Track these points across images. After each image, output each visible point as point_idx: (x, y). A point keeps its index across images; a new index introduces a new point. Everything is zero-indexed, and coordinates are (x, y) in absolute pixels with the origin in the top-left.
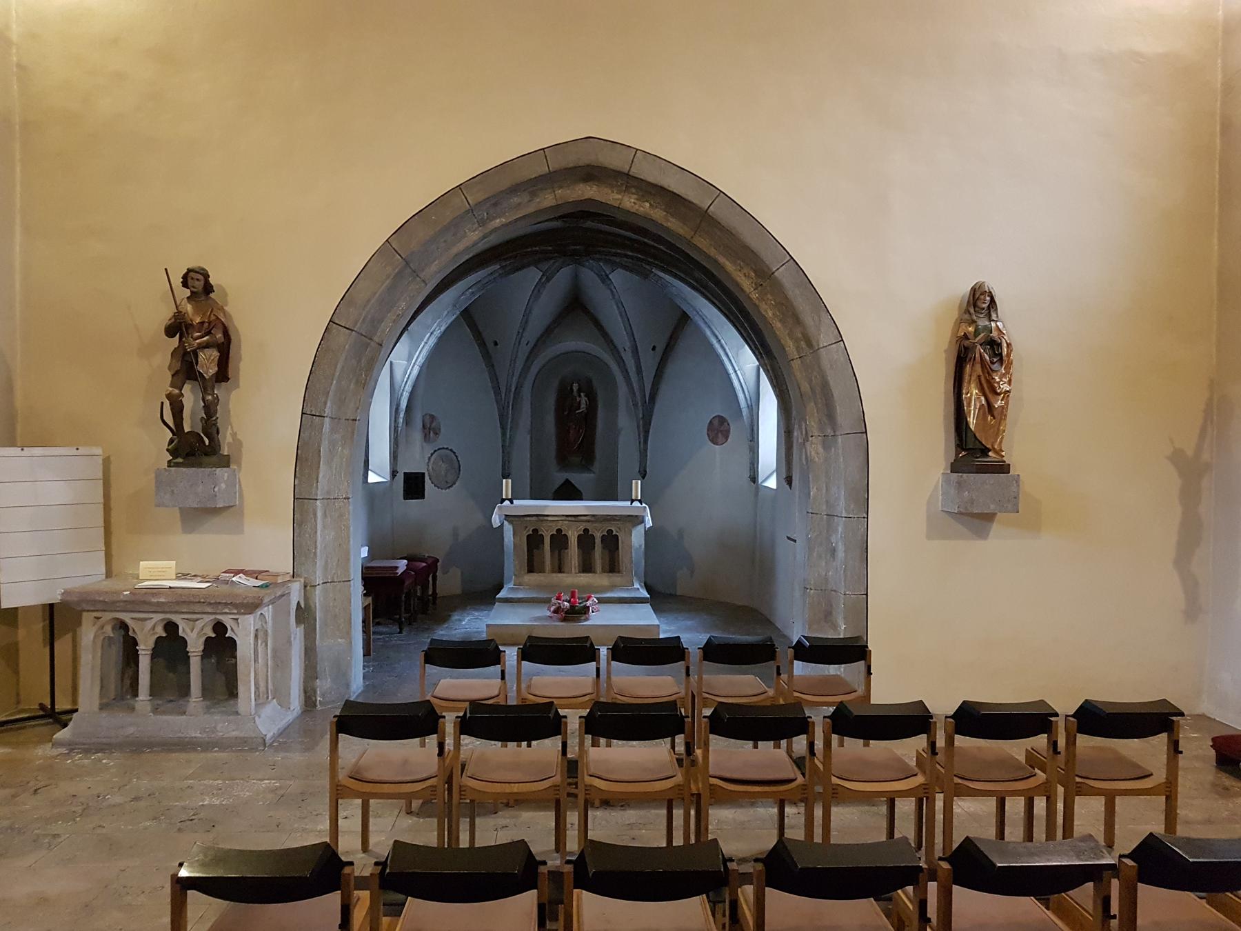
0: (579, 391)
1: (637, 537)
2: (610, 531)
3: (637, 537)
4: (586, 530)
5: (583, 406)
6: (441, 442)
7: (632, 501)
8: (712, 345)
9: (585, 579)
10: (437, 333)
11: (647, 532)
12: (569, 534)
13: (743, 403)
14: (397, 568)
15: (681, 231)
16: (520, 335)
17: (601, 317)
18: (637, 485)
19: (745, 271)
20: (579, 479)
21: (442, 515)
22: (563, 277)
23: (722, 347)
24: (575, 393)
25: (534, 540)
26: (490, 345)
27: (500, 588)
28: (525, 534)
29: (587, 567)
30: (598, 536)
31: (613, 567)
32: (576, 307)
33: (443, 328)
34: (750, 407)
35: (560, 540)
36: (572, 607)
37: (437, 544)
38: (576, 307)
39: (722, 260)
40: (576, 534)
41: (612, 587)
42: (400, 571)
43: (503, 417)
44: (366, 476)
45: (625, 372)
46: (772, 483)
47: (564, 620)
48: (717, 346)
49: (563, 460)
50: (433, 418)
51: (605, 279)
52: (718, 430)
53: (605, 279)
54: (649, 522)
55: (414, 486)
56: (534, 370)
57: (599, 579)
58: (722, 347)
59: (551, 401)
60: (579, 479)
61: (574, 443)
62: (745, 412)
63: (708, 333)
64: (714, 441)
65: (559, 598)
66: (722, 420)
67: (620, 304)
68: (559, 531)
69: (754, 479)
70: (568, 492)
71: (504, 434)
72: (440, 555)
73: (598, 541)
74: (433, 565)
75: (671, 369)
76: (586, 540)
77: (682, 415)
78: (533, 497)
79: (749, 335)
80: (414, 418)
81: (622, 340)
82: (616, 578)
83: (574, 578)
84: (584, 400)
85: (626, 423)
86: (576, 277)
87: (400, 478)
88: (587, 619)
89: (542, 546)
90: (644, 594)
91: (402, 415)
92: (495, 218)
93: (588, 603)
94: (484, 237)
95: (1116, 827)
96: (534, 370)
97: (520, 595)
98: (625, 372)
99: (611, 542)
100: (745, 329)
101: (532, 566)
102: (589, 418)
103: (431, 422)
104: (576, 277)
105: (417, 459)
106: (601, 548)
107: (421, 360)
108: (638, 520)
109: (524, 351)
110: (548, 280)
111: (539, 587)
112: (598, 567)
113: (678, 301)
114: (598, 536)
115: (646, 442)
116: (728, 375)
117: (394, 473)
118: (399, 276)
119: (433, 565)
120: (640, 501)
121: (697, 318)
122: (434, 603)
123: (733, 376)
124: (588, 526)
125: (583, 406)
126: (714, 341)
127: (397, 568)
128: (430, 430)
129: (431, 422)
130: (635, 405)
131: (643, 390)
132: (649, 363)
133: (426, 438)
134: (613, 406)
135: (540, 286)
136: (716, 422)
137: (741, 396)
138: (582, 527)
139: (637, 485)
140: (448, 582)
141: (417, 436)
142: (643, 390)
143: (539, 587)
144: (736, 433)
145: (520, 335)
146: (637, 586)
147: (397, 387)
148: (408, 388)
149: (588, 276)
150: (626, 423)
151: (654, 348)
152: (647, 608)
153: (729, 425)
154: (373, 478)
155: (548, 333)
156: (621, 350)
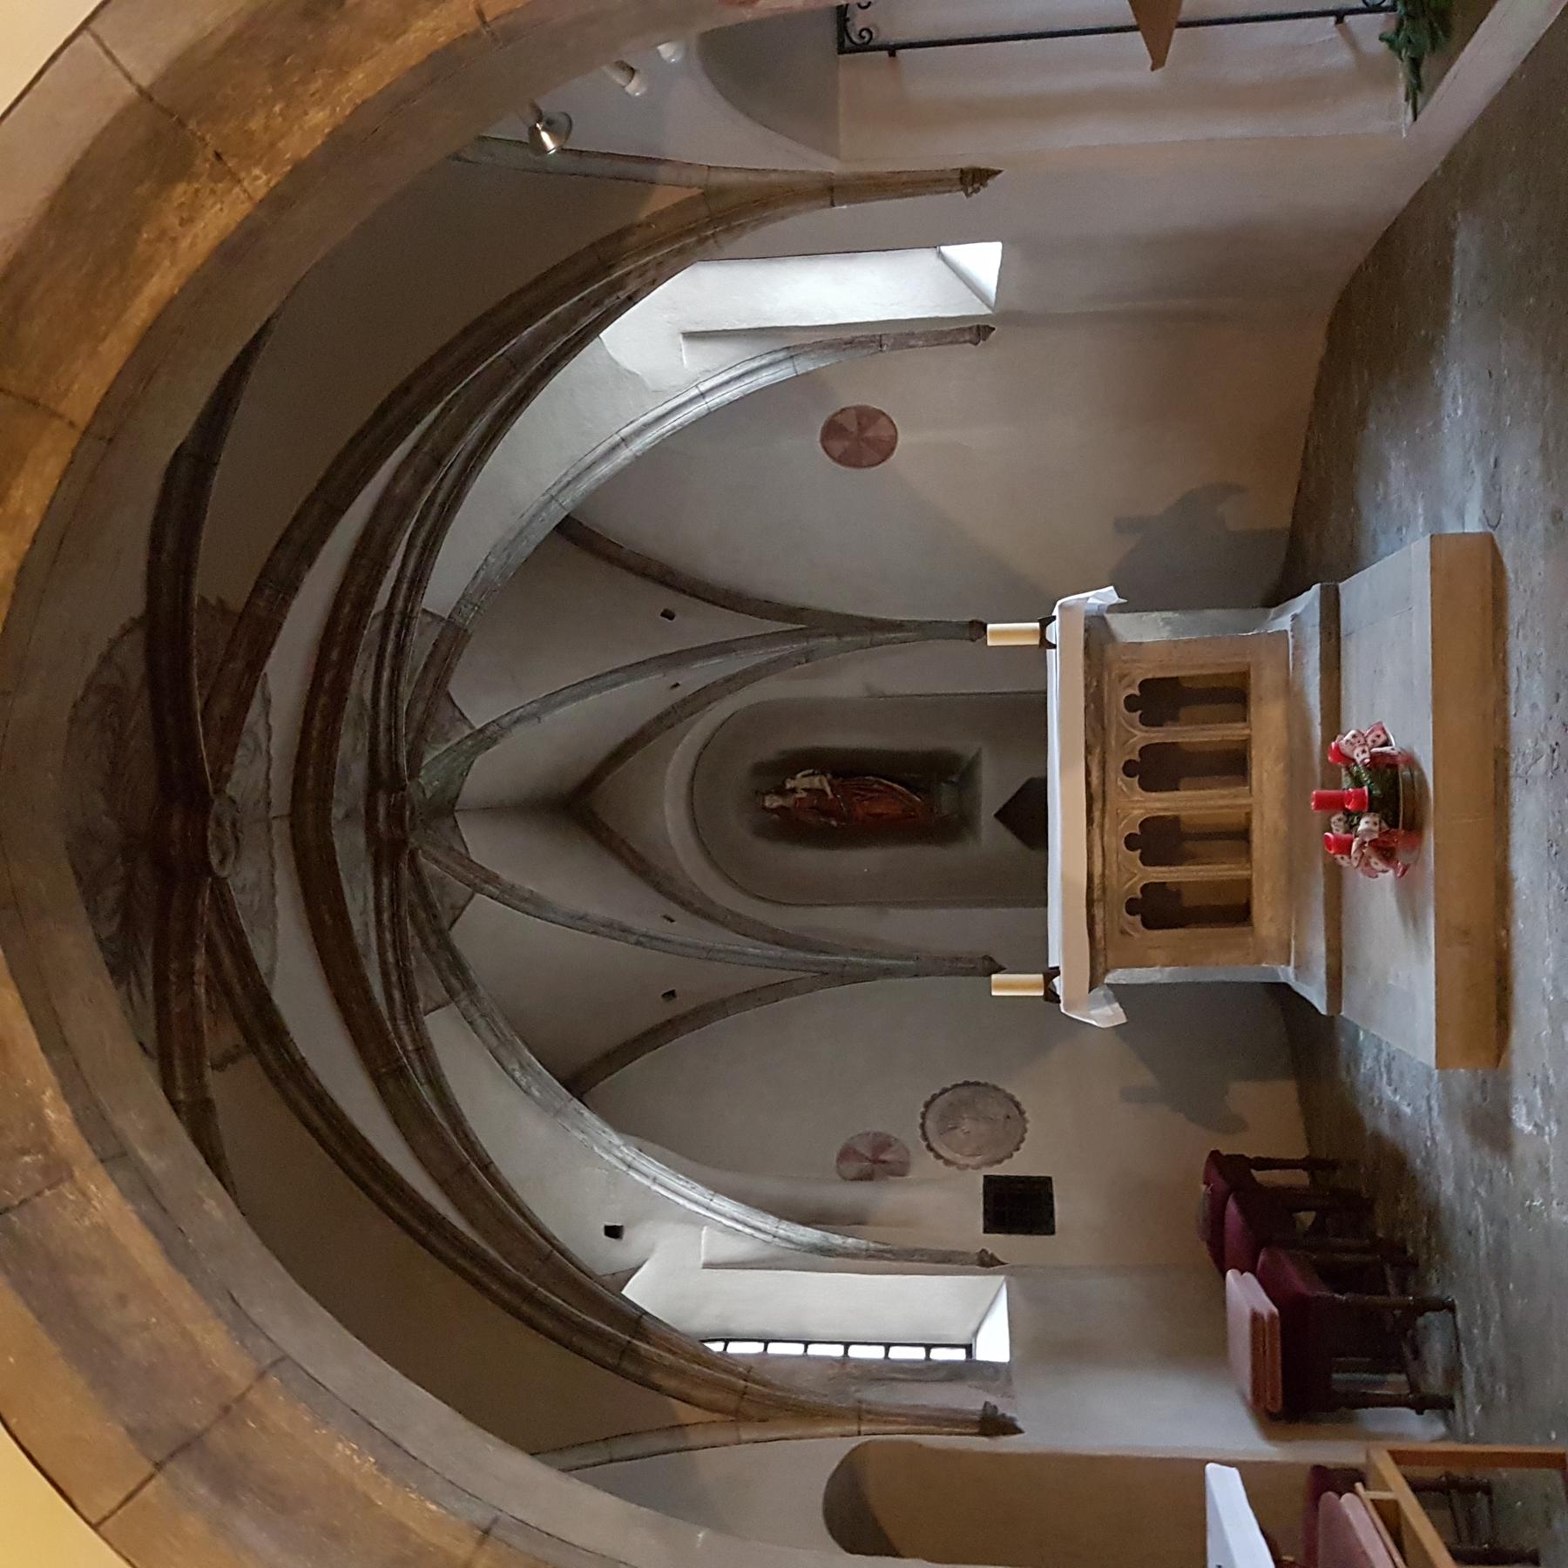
0: (781, 791)
1: (1146, 632)
2: (1131, 703)
3: (1146, 632)
4: (1129, 769)
5: (816, 782)
6: (910, 1136)
7: (1046, 644)
8: (638, 459)
9: (1267, 769)
10: (629, 1153)
11: (1134, 602)
12: (1139, 814)
13: (784, 372)
14: (1256, 1318)
15: (53, 468)
16: (645, 941)
17: (601, 753)
18: (1005, 633)
19: (172, 220)
20: (993, 789)
21: (1097, 1140)
22: (482, 843)
23: (639, 432)
24: (789, 802)
25: (1159, 909)
26: (681, 1006)
27: (1282, 994)
28: (1140, 934)
29: (1233, 764)
30: (1142, 736)
31: (1232, 694)
32: (579, 807)
33: (616, 1140)
34: (793, 353)
35: (1156, 841)
36: (1373, 805)
37: (1175, 1151)
38: (579, 807)
39: (140, 312)
40: (1139, 795)
41: (1291, 692)
42: (1266, 1306)
43: (845, 976)
44: (992, 1370)
45: (732, 683)
46: (982, 261)
47: (1414, 827)
48: (637, 446)
49: (951, 828)
50: (846, 1154)
51: (485, 739)
52: (858, 439)
53: (485, 739)
54: (1107, 596)
55: (1018, 1206)
56: (726, 897)
57: (1267, 729)
58: (639, 432)
59: (810, 860)
60: (993, 789)
61: (907, 799)
62: (805, 365)
63: (604, 469)
64: (885, 449)
65: (1344, 847)
66: (832, 430)
67: (551, 701)
68: (1130, 842)
69: (978, 331)
70: (1027, 815)
71: (888, 972)
72: (1199, 1144)
73: (1158, 735)
74: (1230, 1173)
75: (717, 568)
76: (1154, 769)
77: (815, 534)
78: (1044, 903)
79: (560, 325)
80: (839, 1217)
81: (641, 698)
82: (1265, 681)
83: (1266, 794)
84: (802, 782)
85: (850, 679)
86: (495, 810)
87: (999, 1243)
88: (1411, 762)
89: (1174, 890)
90: (1308, 602)
91: (837, 1240)
92: (40, 1119)
93: (1361, 756)
94: (115, 1156)
95: (943, 911)
96: (726, 897)
97: (1318, 947)
98: (732, 683)
99: (1160, 698)
100: (543, 338)
101: (1234, 911)
102: (848, 769)
103: (860, 1157)
104: (495, 810)
105: (949, 1200)
106: (1175, 725)
107: (698, 1193)
108: (1096, 631)
109: (687, 930)
110: (493, 879)
111: (1293, 891)
112: (1227, 733)
113: (526, 548)
114: (1142, 736)
115: (899, 626)
116: (710, 414)
117: (987, 1262)
118: (228, 1480)
119: (1230, 1173)
120: (1046, 622)
121: (568, 501)
122: (1333, 1165)
123: (714, 401)
124: (1116, 764)
125: (816, 782)
126: (625, 454)
127: (1256, 1318)
128: (875, 1161)
129: (860, 1157)
130: (808, 656)
131: (766, 639)
132: (702, 624)
133: (899, 1170)
134: (814, 712)
135: (509, 896)
136: (838, 446)
137: (765, 378)
138: (1118, 781)
139: (1005, 633)
140: (1267, 1122)
141: (887, 1197)
142: (766, 639)
143: (1293, 891)
144: (857, 390)
145: (645, 941)
146: (1284, 623)
147: (767, 1252)
148: (769, 1223)
149: (488, 776)
150: (850, 679)
151: (668, 615)
152: (1354, 591)
153: (840, 403)
154: (994, 1345)
155: (643, 867)
156: (679, 694)
